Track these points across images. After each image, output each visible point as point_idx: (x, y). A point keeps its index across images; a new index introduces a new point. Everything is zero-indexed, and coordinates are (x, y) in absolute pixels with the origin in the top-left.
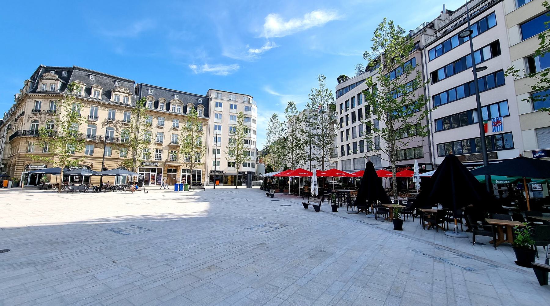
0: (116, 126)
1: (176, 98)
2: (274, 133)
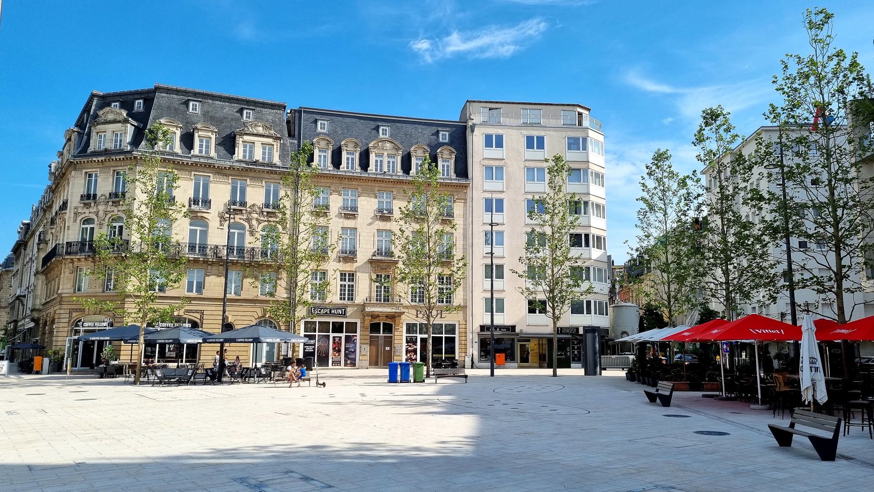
0: (248, 220)
1: (384, 136)
2: (660, 209)
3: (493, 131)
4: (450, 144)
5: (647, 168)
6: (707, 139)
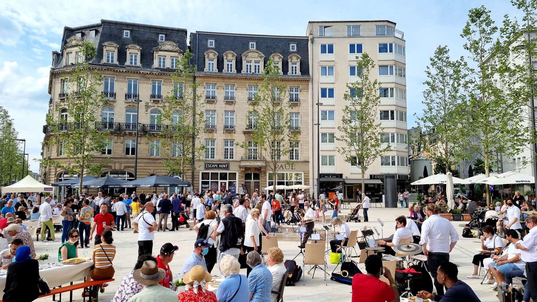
1: (252, 49)
2: (441, 89)
3: (327, 42)
4: (298, 52)
5: (431, 60)
6: (473, 32)
